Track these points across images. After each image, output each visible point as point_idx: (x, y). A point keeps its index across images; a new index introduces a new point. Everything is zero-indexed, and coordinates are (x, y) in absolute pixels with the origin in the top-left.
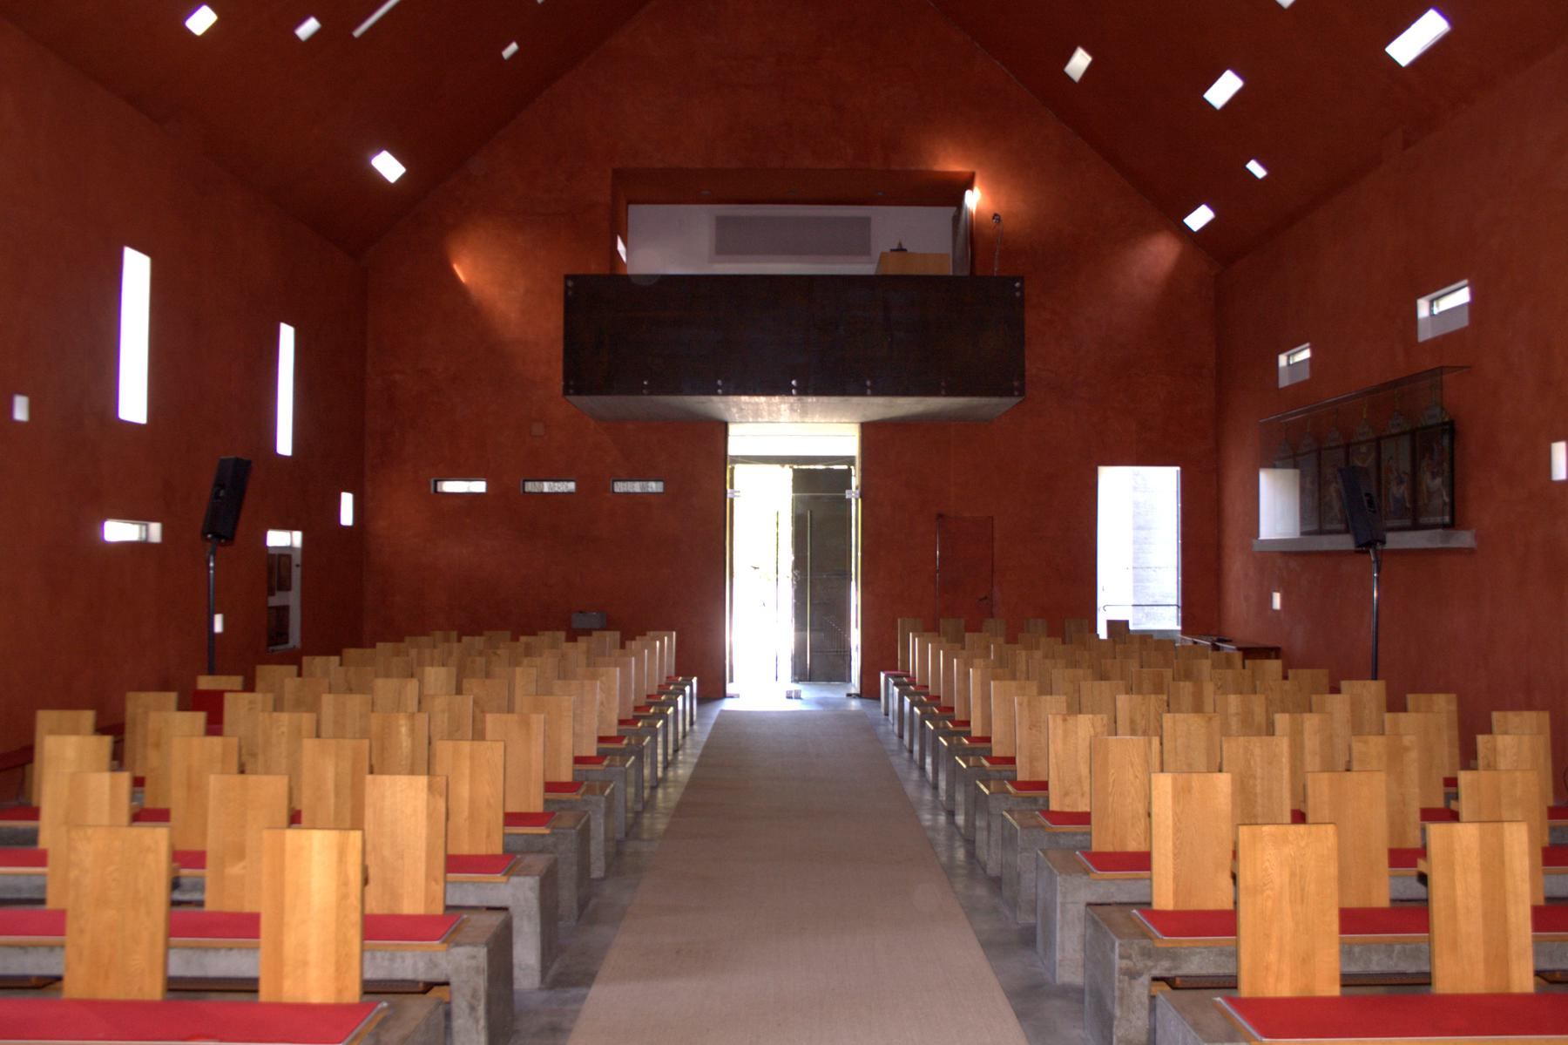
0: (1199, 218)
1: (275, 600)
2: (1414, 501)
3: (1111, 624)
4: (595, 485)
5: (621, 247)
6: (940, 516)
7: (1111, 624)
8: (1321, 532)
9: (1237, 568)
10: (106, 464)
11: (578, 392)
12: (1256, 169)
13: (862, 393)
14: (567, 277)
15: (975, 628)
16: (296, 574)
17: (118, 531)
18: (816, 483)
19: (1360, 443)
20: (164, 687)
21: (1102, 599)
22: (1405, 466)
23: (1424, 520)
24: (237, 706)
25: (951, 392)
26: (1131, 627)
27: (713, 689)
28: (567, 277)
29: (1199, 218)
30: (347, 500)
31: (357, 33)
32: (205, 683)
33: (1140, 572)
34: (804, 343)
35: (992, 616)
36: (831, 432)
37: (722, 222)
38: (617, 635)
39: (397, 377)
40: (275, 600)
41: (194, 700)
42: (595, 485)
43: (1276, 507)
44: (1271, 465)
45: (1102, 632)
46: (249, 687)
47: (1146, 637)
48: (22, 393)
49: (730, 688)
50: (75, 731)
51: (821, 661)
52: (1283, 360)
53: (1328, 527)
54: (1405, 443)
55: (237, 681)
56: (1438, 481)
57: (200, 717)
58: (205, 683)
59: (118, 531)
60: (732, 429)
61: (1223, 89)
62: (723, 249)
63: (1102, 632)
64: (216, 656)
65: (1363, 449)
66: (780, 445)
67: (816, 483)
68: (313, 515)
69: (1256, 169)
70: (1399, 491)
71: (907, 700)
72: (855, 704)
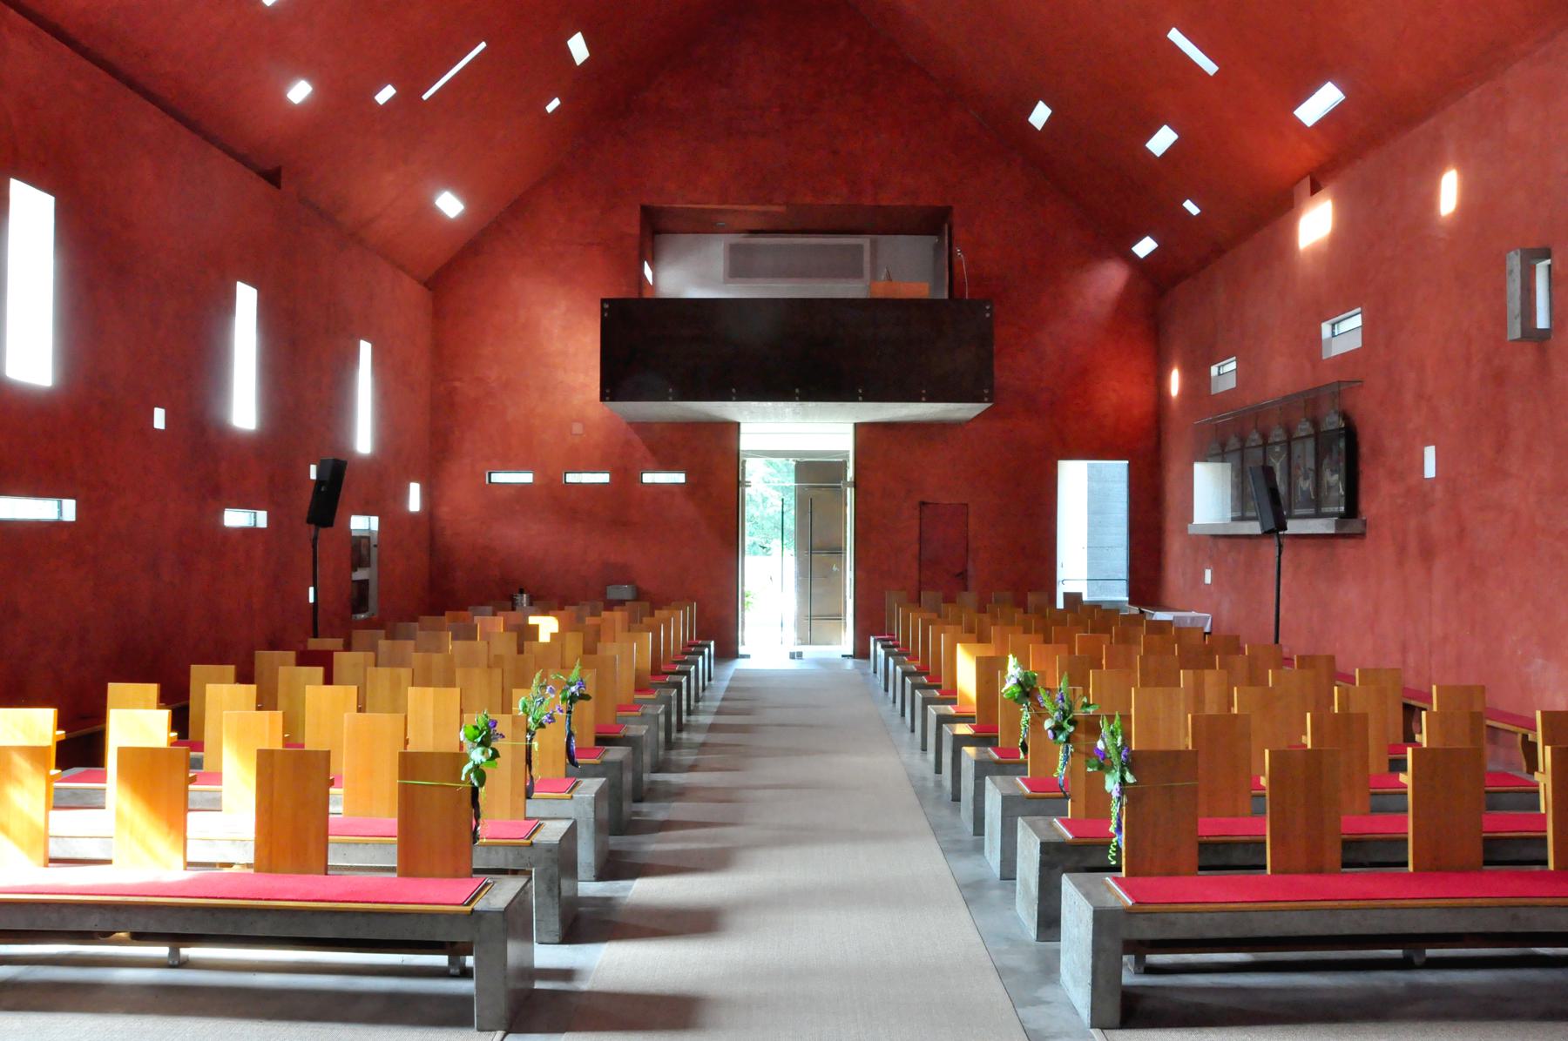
0: (1145, 247)
1: (360, 575)
2: (1317, 492)
3: (1066, 595)
4: (625, 476)
5: (648, 272)
6: (923, 504)
7: (1066, 595)
8: (1243, 518)
9: (1175, 548)
10: (214, 465)
11: (612, 400)
12: (1191, 208)
13: (855, 400)
14: (603, 301)
15: (949, 599)
16: (374, 553)
17: (235, 518)
18: (815, 474)
19: (1276, 443)
20: (220, 660)
21: (1060, 575)
22: (1311, 463)
23: (1325, 510)
24: (343, 660)
25: (931, 399)
26: (1085, 598)
27: (728, 651)
28: (603, 301)
29: (1145, 247)
30: (415, 490)
31: (425, 97)
32: (314, 644)
33: (1095, 550)
34: (803, 357)
35: (966, 589)
36: (828, 429)
37: (733, 249)
38: (647, 604)
39: (457, 384)
40: (360, 575)
41: (306, 659)
42: (625, 476)
43: (1209, 495)
44: (1204, 458)
45: (1060, 604)
46: (348, 647)
47: (1095, 606)
48: (160, 406)
49: (742, 650)
50: (221, 681)
51: (815, 617)
52: (1214, 370)
53: (1248, 514)
54: (1310, 444)
55: (339, 642)
56: (1336, 477)
57: (319, 671)
58: (314, 644)
59: (235, 518)
60: (743, 428)
61: (1162, 141)
62: (737, 271)
63: (1060, 604)
64: (315, 621)
65: (1277, 449)
66: (785, 440)
67: (815, 474)
68: (383, 501)
69: (1191, 208)
70: (1305, 485)
71: (891, 660)
72: (850, 663)
